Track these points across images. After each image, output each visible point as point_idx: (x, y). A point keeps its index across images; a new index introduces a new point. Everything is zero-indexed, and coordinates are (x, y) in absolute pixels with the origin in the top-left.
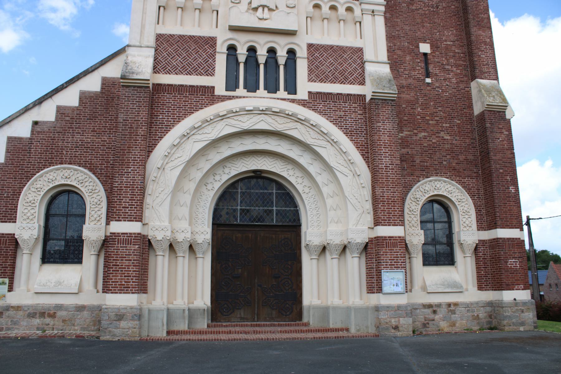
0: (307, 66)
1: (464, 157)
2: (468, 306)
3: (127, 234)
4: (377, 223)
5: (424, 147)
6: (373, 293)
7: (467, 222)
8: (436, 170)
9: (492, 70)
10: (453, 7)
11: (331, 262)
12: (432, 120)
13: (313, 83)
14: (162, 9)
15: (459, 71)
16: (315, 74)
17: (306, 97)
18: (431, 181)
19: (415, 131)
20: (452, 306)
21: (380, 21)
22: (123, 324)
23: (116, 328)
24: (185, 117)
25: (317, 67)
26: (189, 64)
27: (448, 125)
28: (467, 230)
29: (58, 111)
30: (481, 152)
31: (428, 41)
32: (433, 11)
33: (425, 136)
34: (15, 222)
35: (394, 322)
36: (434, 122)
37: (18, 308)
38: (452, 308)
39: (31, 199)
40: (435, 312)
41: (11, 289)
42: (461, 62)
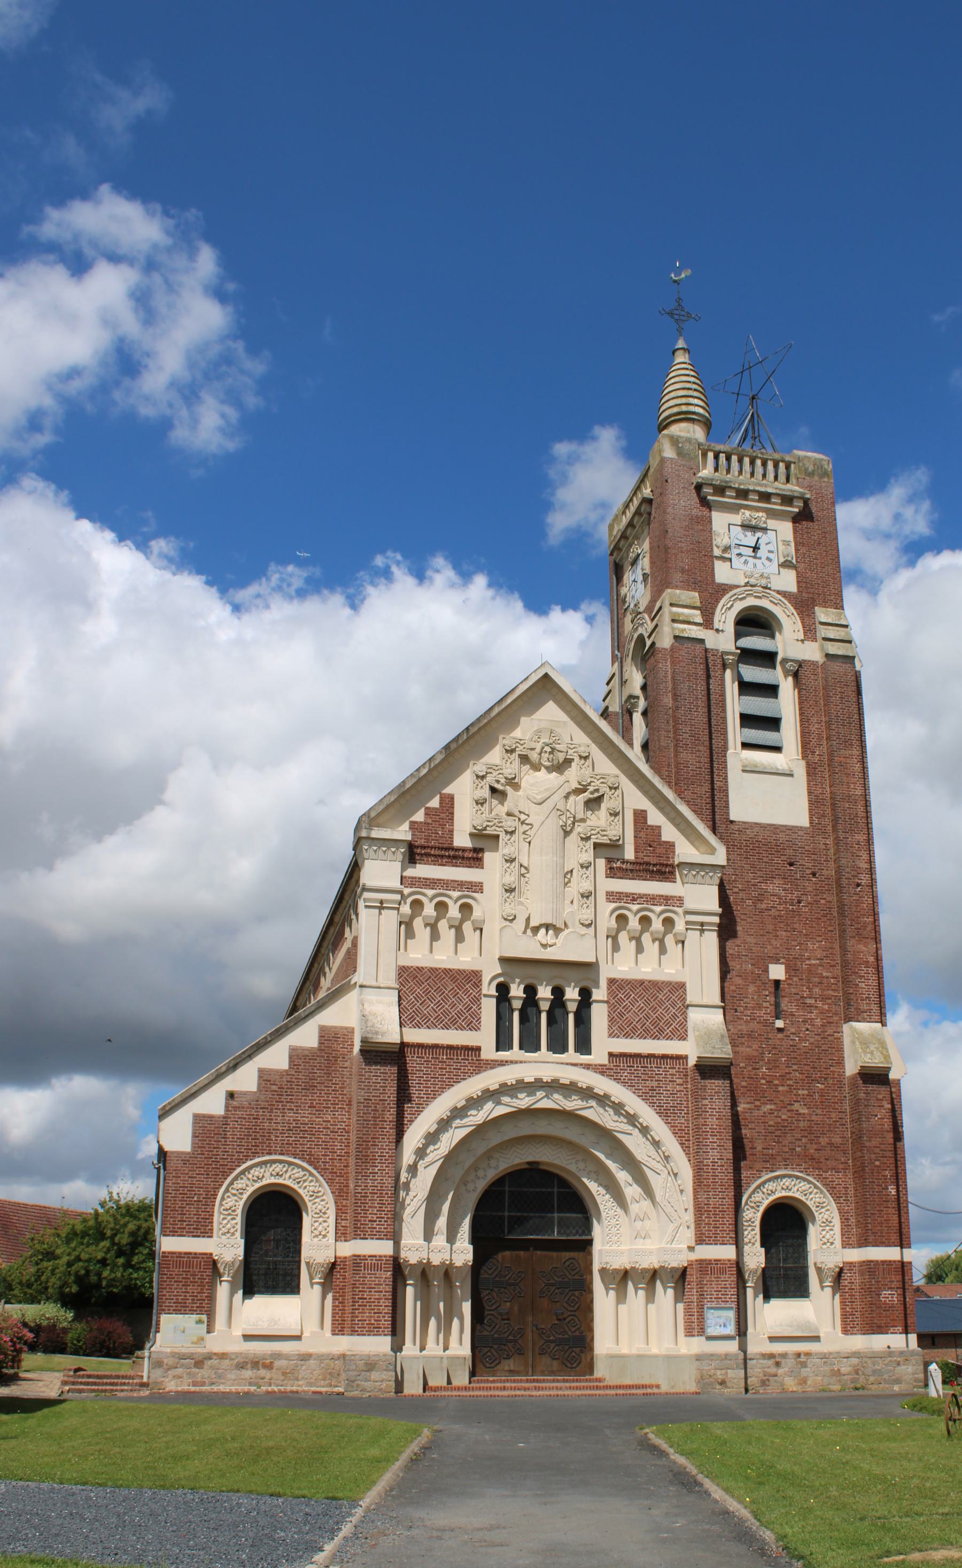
0: (606, 1013)
1: (827, 1140)
3: (375, 1256)
4: (700, 1240)
6: (693, 1336)
8: (785, 1160)
9: (875, 1008)
10: (823, 901)
11: (636, 1296)
13: (615, 1039)
15: (826, 1007)
16: (619, 1027)
17: (604, 1060)
19: (757, 1103)
20: (802, 1356)
22: (375, 1375)
23: (367, 1380)
25: (621, 1015)
26: (446, 1013)
27: (806, 1092)
29: (260, 1077)
30: (852, 1133)
32: (793, 911)
34: (211, 1237)
35: (720, 1375)
36: (785, 1088)
37: (223, 1356)
38: (803, 1359)
39: (231, 1204)
40: (778, 1364)
41: (208, 1332)
42: (831, 993)
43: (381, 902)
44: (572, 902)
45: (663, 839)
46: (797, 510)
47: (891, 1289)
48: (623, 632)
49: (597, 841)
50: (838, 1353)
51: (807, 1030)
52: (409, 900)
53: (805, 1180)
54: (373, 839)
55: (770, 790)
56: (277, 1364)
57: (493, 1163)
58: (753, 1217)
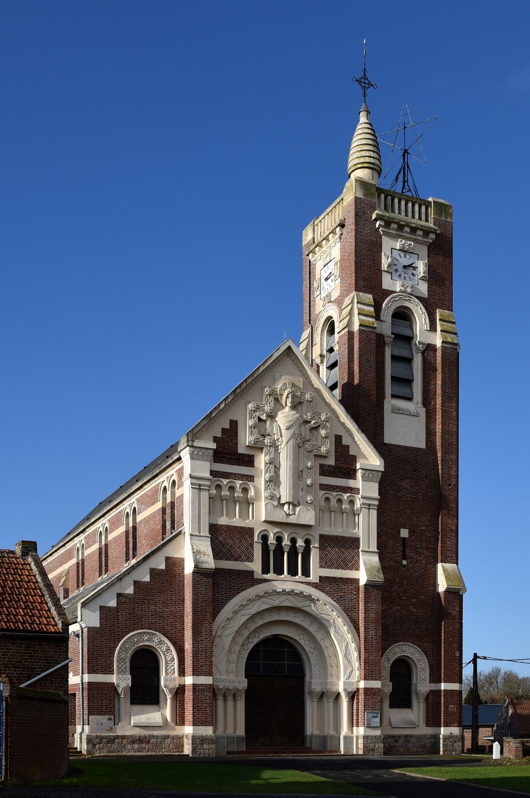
1: (425, 626)
2: (419, 737)
3: (204, 685)
5: (397, 618)
7: (423, 677)
9: (454, 555)
10: (430, 493)
12: (404, 596)
14: (211, 499)
15: (428, 554)
16: (325, 563)
18: (400, 645)
21: (374, 514)
24: (234, 596)
28: (422, 684)
31: (407, 527)
33: (398, 609)
37: (123, 737)
39: (123, 656)
43: (200, 486)
44: (302, 489)
45: (350, 454)
46: (431, 241)
47: (454, 704)
48: (315, 311)
49: (316, 453)
50: (425, 736)
51: (418, 566)
52: (215, 484)
53: (413, 647)
54: (195, 447)
55: (406, 427)
56: (152, 740)
57: (257, 635)
58: (386, 665)
